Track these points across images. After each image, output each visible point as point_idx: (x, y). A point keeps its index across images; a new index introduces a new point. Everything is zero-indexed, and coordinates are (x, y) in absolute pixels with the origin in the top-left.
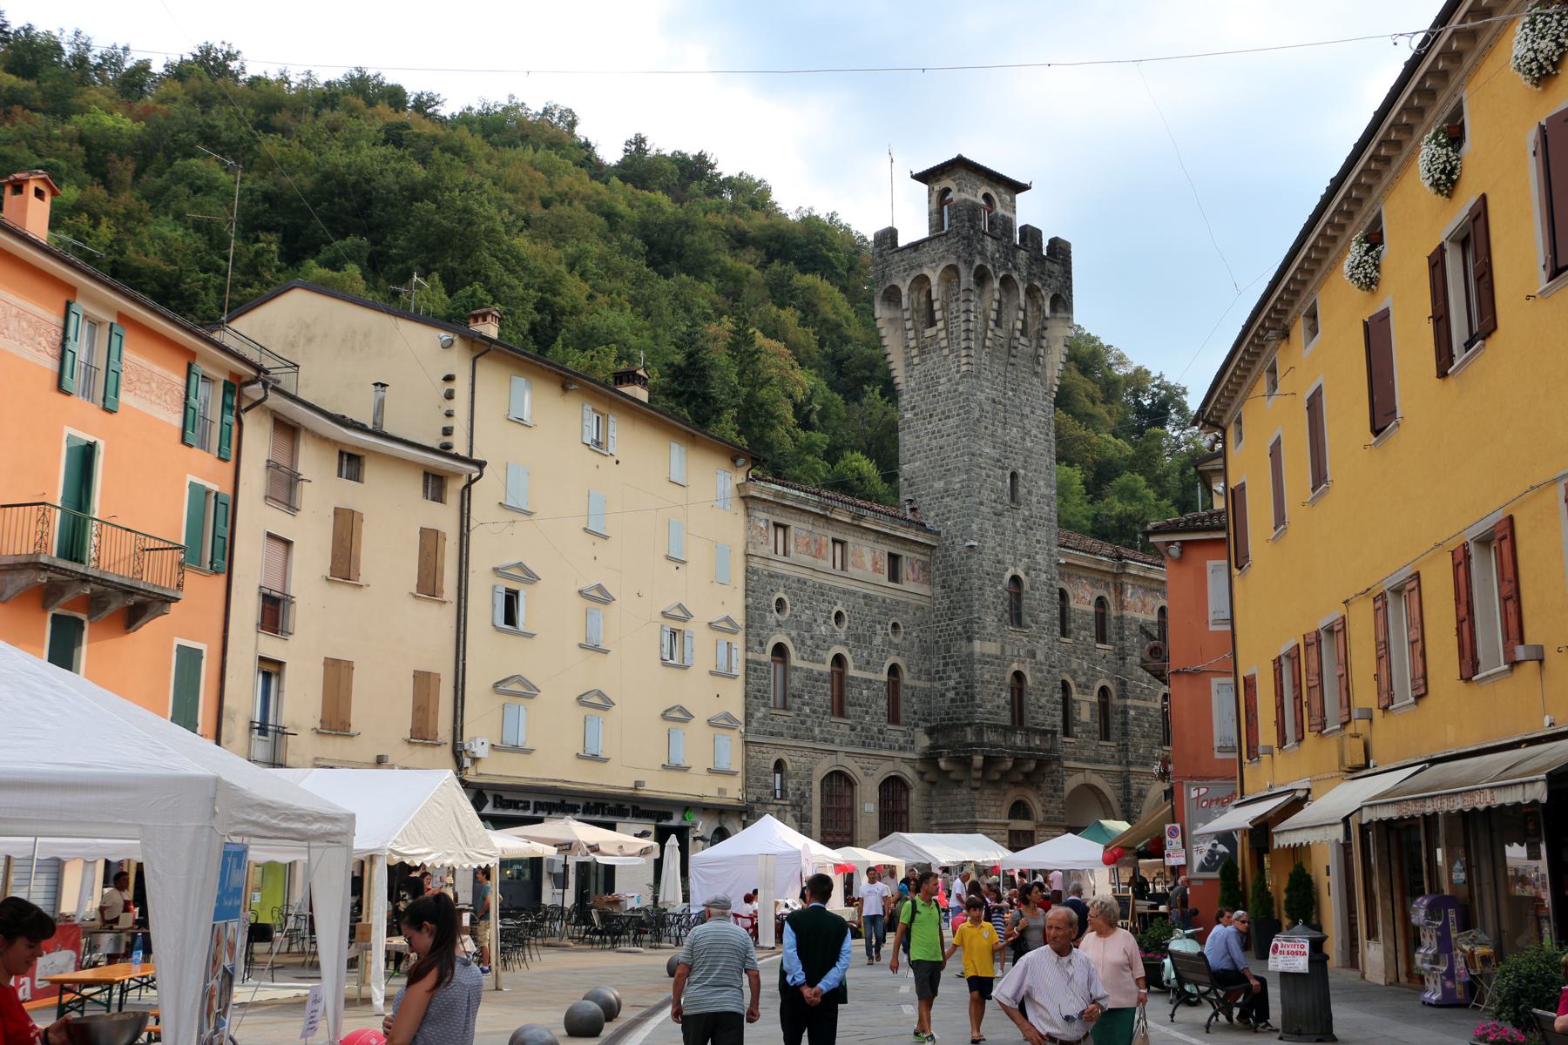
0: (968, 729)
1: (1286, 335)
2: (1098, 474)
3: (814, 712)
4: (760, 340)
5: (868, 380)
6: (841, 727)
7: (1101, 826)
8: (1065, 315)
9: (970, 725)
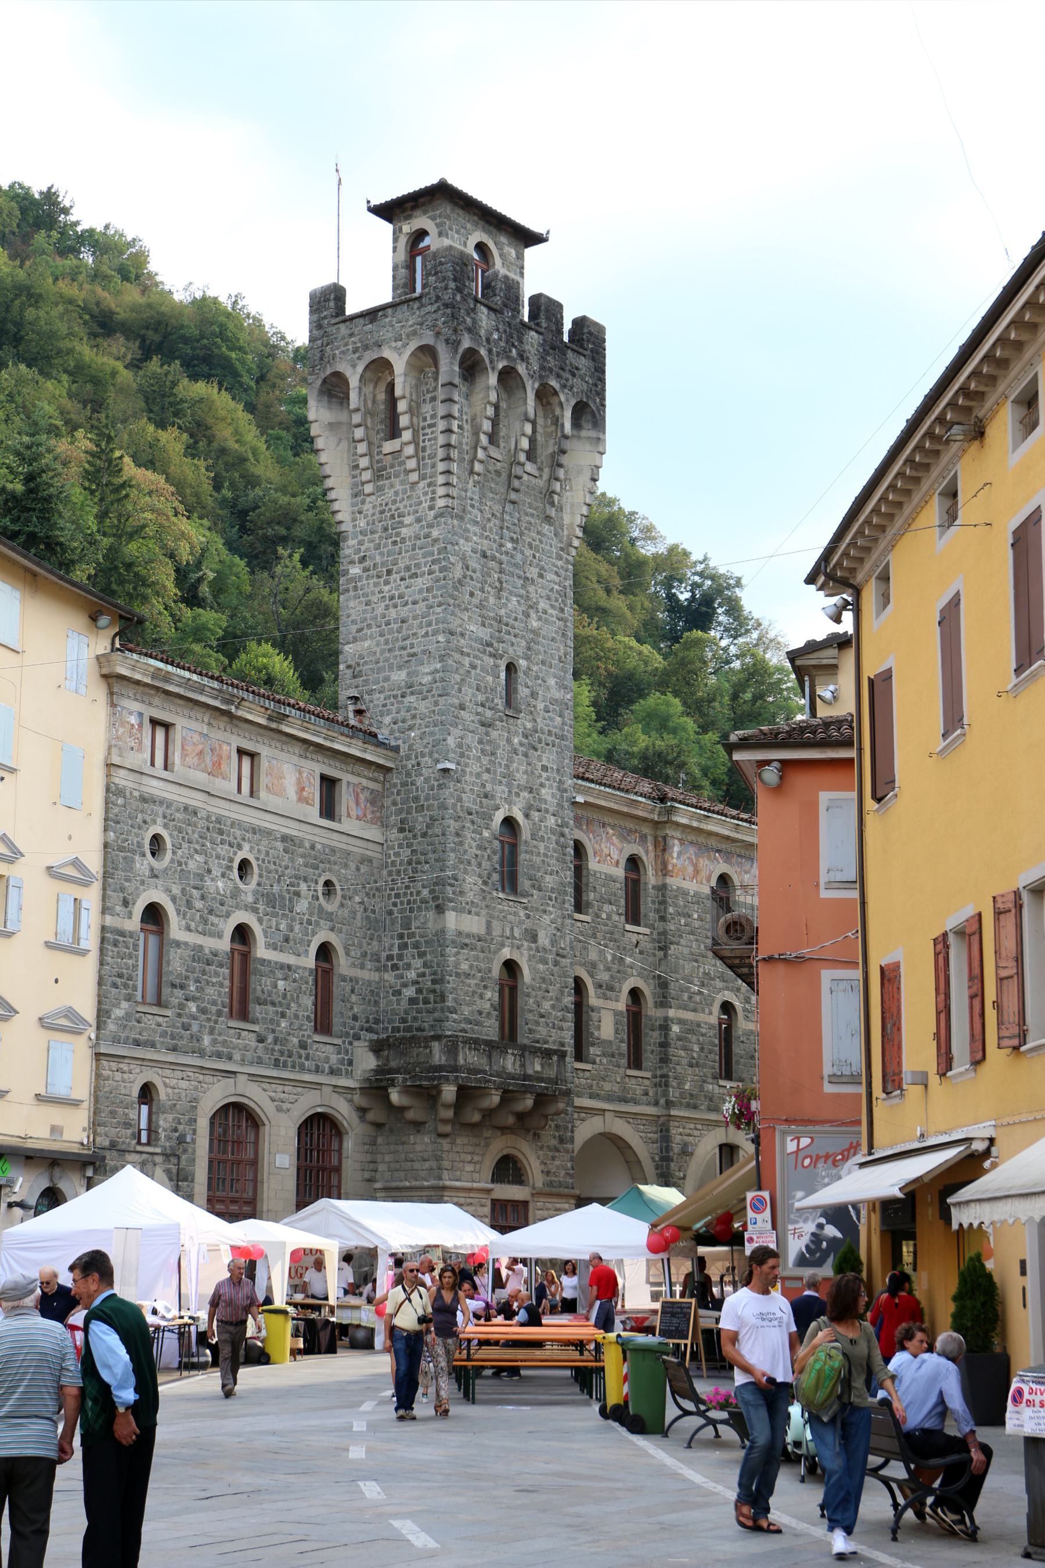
0: (436, 1046)
1: (979, 433)
2: (613, 693)
3: (203, 1011)
4: (130, 469)
5: (284, 540)
6: (243, 1038)
7: (640, 1193)
8: (592, 434)
9: (437, 1038)
